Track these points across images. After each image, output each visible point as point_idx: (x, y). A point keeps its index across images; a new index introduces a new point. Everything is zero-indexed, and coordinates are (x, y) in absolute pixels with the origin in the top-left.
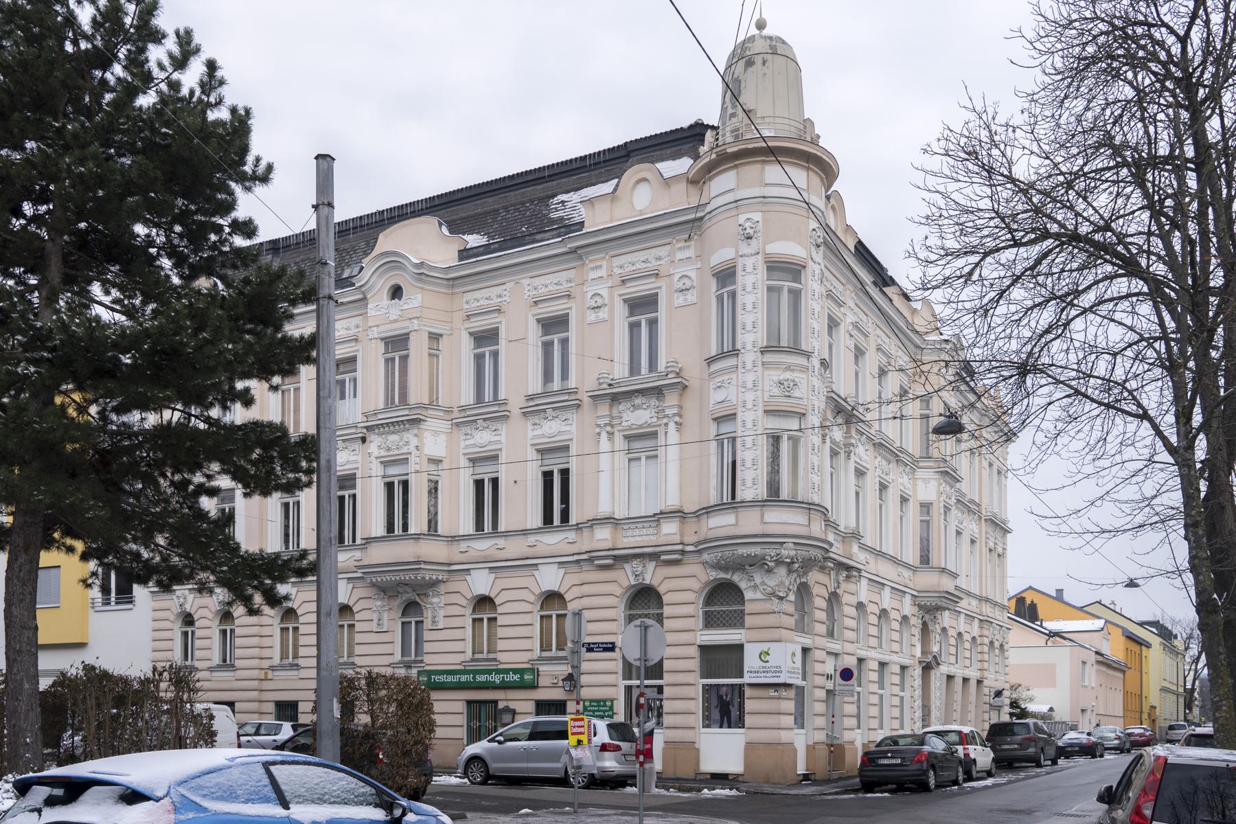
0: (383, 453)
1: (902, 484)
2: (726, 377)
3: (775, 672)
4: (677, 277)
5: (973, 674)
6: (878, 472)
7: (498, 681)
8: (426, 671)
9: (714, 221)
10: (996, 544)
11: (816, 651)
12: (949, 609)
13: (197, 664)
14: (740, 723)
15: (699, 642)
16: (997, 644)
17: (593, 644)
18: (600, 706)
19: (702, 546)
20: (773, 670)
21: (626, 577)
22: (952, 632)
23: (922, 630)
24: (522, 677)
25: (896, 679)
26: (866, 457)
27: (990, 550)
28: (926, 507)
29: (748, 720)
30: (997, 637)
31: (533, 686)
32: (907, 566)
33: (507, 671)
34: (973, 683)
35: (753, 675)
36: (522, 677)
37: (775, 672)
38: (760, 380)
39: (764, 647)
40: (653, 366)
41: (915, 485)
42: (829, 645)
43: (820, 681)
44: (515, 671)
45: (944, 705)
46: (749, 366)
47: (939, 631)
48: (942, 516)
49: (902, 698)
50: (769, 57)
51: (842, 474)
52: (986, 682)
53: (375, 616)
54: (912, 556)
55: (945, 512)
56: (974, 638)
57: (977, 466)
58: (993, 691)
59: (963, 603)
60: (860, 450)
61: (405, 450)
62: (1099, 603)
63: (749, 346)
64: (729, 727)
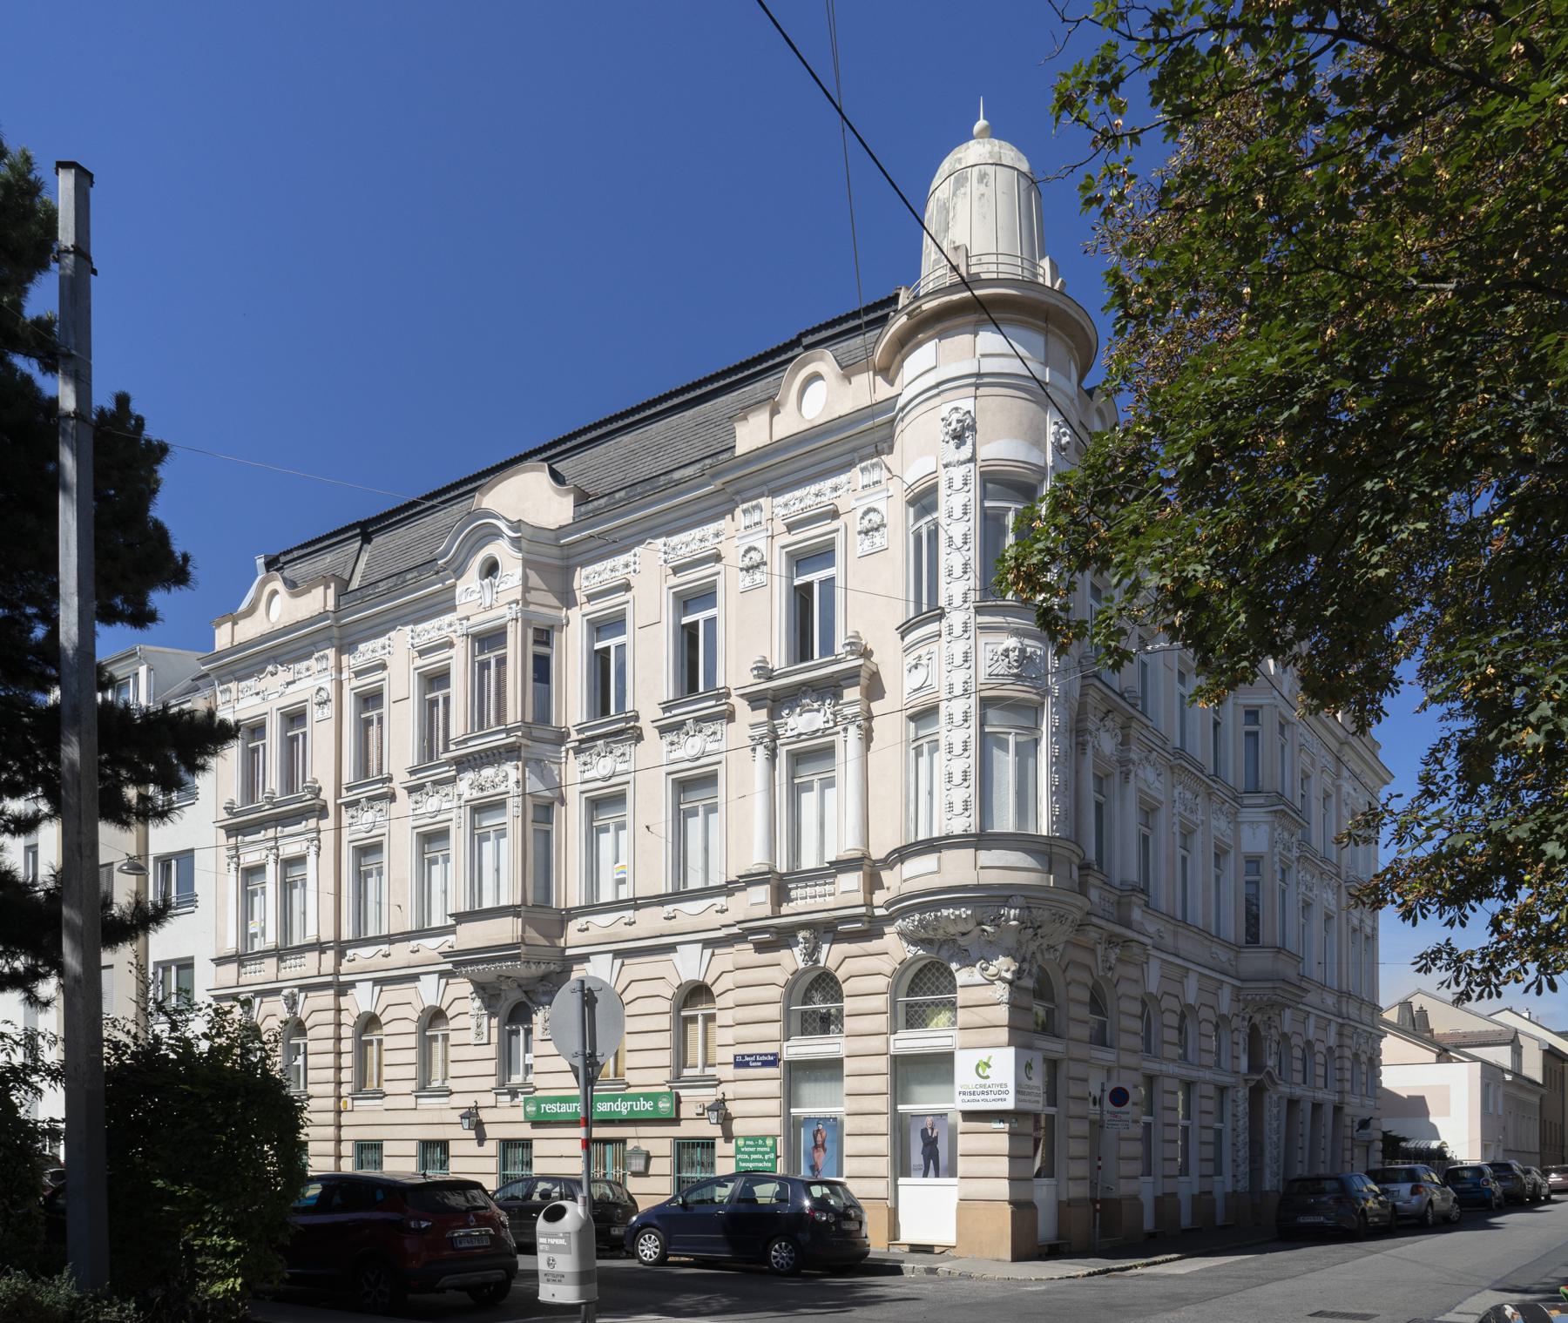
0: (476, 794)
1: (1218, 829)
2: (923, 651)
3: (999, 1093)
4: (859, 512)
5: (1328, 1097)
6: (1178, 807)
7: (625, 1112)
8: (536, 1097)
9: (907, 420)
10: (1361, 921)
11: (1166, 1080)
12: (1289, 1007)
13: (311, 1090)
14: (952, 1172)
15: (892, 1051)
16: (1364, 1058)
17: (749, 1056)
18: (757, 1146)
19: (903, 907)
20: (995, 1089)
21: (792, 959)
22: (1296, 1040)
23: (1250, 1036)
24: (655, 1106)
25: (1209, 1105)
26: (1157, 784)
27: (1354, 930)
28: (1254, 862)
29: (963, 1165)
30: (1364, 1047)
31: (676, 1121)
32: (1225, 944)
33: (636, 1097)
34: (1328, 1111)
35: (967, 1098)
36: (655, 1106)
37: (999, 1093)
38: (973, 649)
39: (983, 1055)
40: (827, 647)
41: (1237, 831)
42: (1145, 1064)
43: (1075, 1109)
44: (647, 1097)
45: (1282, 1143)
46: (958, 630)
47: (1276, 1038)
48: (1279, 876)
49: (1219, 1133)
50: (991, 170)
51: (1117, 805)
52: (1347, 1110)
53: (472, 1023)
54: (1233, 927)
55: (1283, 871)
56: (1330, 1049)
57: (1334, 812)
58: (1357, 1120)
59: (1311, 998)
60: (1149, 774)
61: (502, 789)
62: (1510, 1010)
63: (957, 601)
64: (937, 1175)
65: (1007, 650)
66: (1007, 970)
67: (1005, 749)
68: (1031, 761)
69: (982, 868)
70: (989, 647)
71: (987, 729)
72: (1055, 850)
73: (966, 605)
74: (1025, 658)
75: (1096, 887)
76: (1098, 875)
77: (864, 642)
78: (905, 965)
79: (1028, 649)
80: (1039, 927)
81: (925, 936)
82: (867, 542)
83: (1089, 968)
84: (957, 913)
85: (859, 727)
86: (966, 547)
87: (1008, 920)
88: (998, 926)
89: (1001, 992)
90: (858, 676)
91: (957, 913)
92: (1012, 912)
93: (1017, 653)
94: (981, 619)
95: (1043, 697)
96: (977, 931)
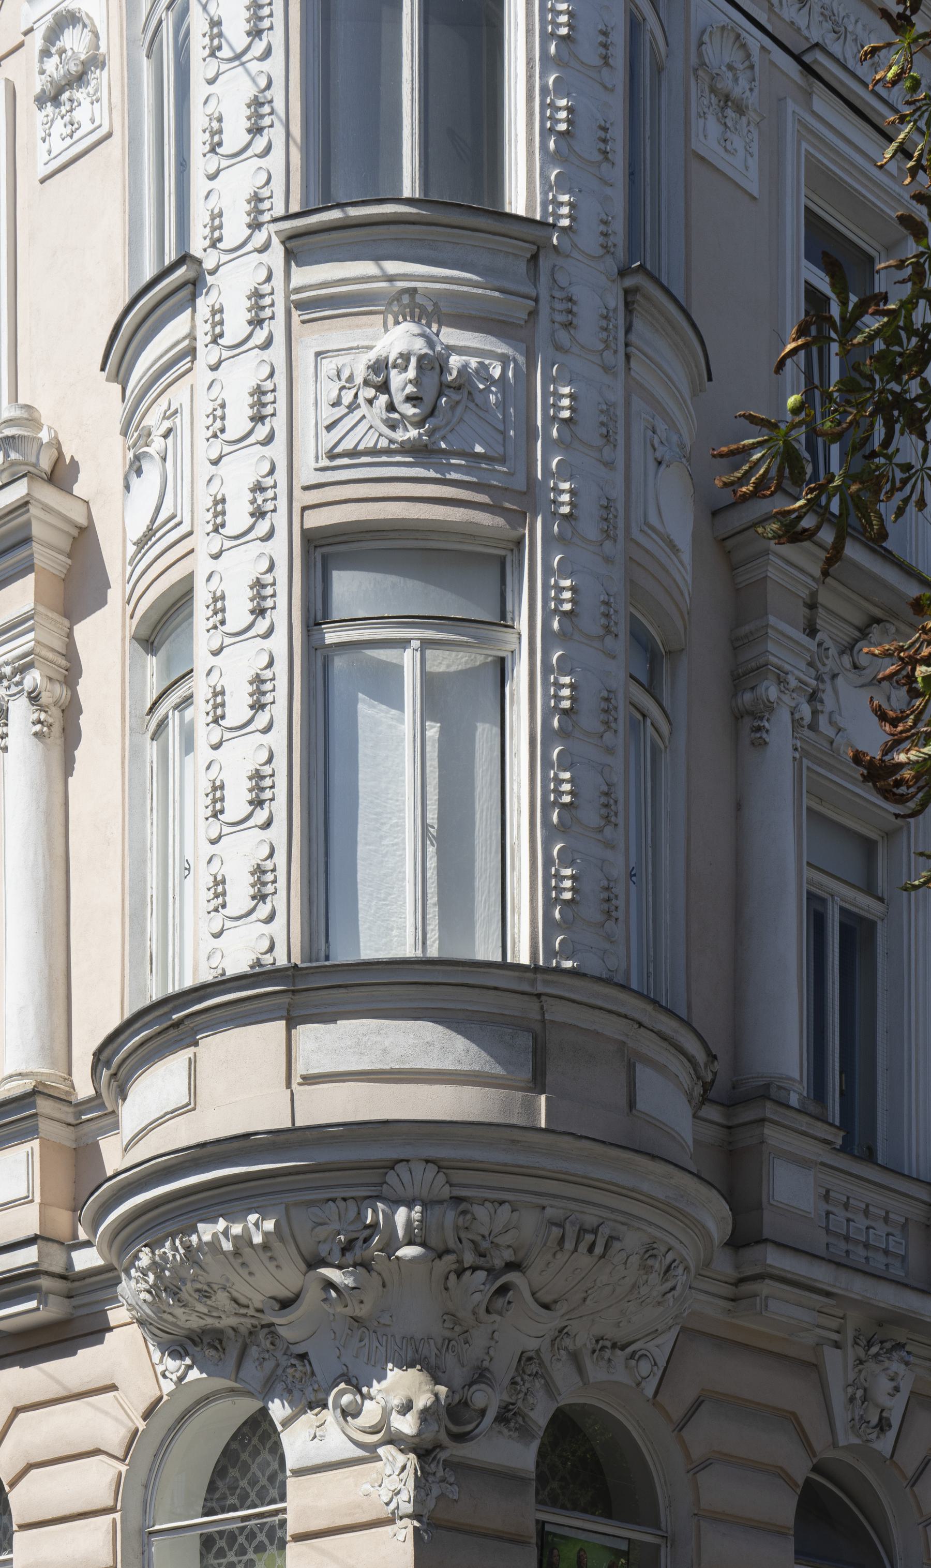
38: (280, 378)
65: (380, 367)
66: (406, 1408)
67: (395, 701)
68: (485, 733)
69: (308, 1080)
70: (329, 366)
71: (332, 636)
72: (558, 1013)
73: (260, 238)
74: (443, 388)
75: (803, 1163)
76: (803, 1122)
77: (44, 436)
78: (164, 1419)
79: (455, 361)
80: (512, 1266)
81: (195, 1323)
82: (59, 127)
83: (792, 1420)
84: (237, 1229)
85: (34, 698)
86: (259, 47)
87: (389, 1246)
88: (365, 1265)
89: (393, 1483)
90: (27, 540)
91: (237, 1229)
92: (401, 1215)
93: (411, 373)
94: (304, 276)
95: (518, 518)
96: (313, 1294)
